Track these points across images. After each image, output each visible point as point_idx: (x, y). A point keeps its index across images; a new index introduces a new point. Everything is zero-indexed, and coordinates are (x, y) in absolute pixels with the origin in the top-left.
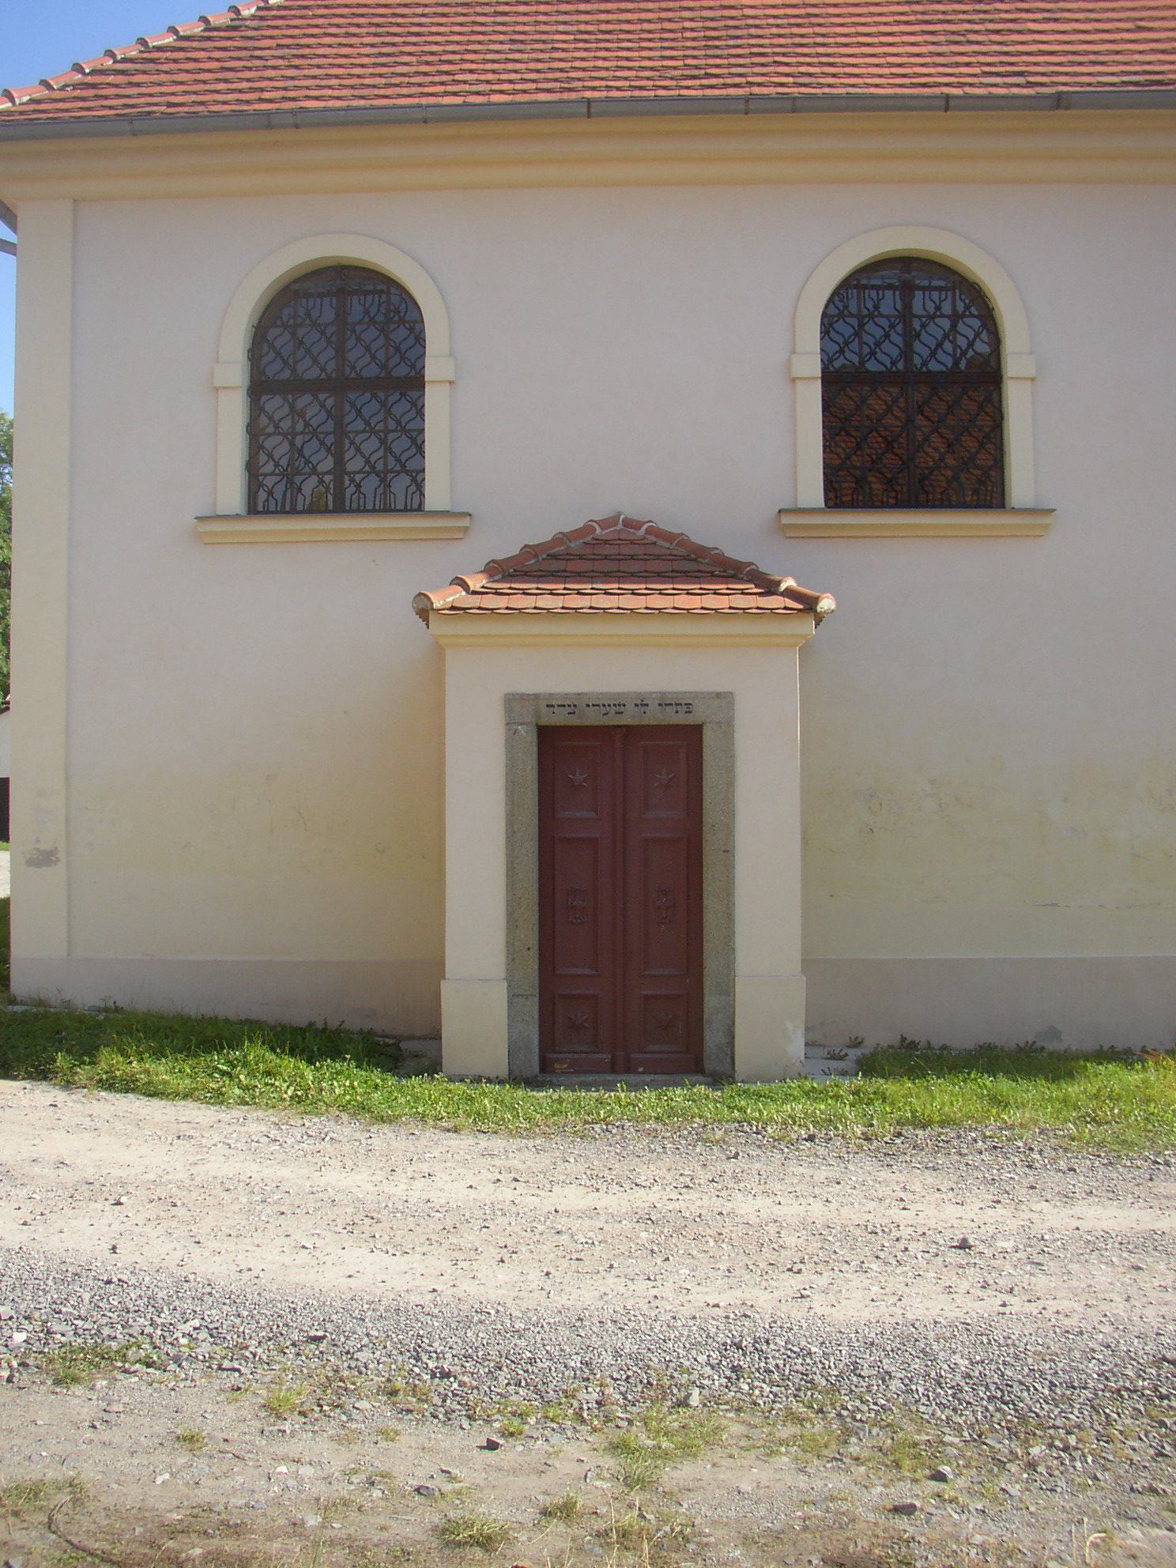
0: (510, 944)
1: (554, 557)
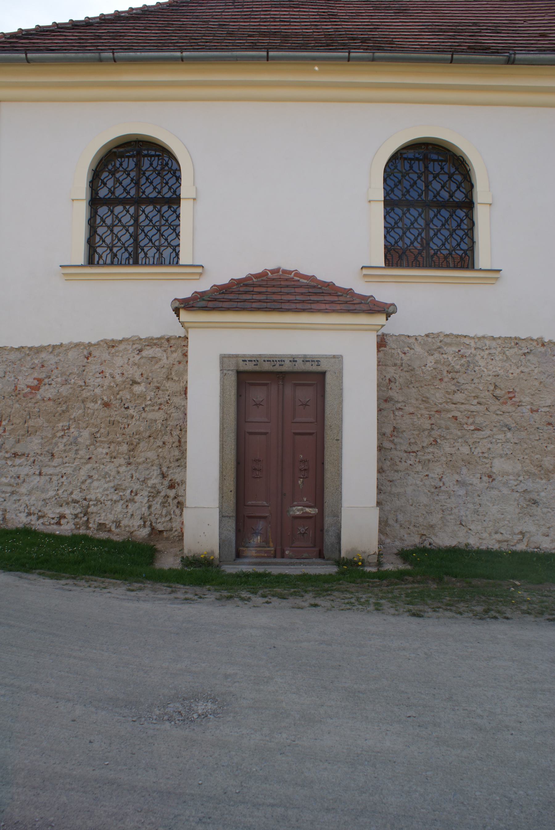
1: (246, 285)
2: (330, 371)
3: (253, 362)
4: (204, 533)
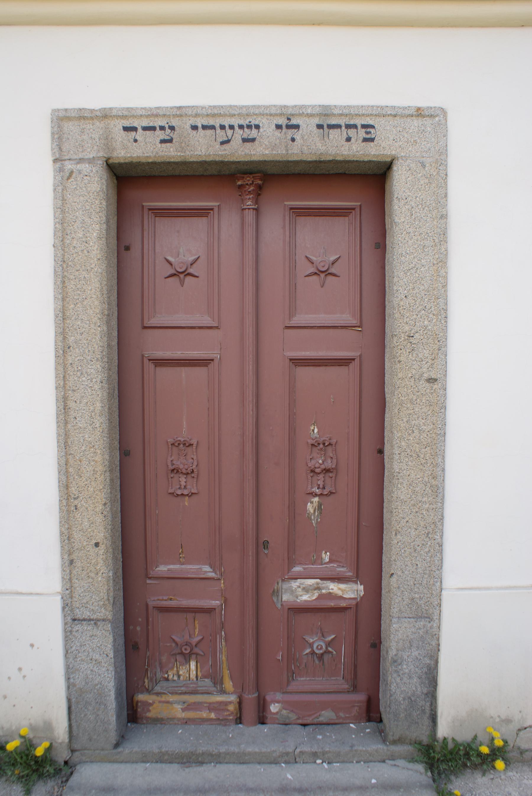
2: (405, 158)
3: (158, 132)
4: (20, 669)
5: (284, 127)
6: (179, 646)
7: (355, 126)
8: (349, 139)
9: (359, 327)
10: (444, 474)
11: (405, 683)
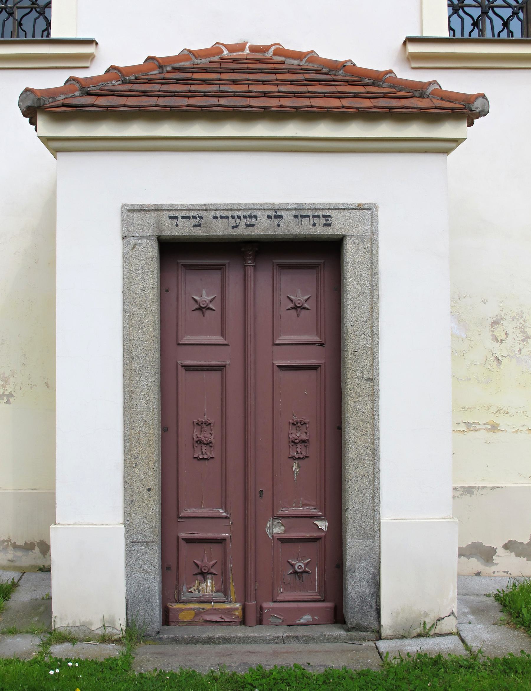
0: (127, 485)
3: (192, 220)
5: (273, 217)
6: (200, 568)
7: (318, 216)
8: (314, 225)
9: (323, 344)
10: (379, 441)
11: (358, 586)
